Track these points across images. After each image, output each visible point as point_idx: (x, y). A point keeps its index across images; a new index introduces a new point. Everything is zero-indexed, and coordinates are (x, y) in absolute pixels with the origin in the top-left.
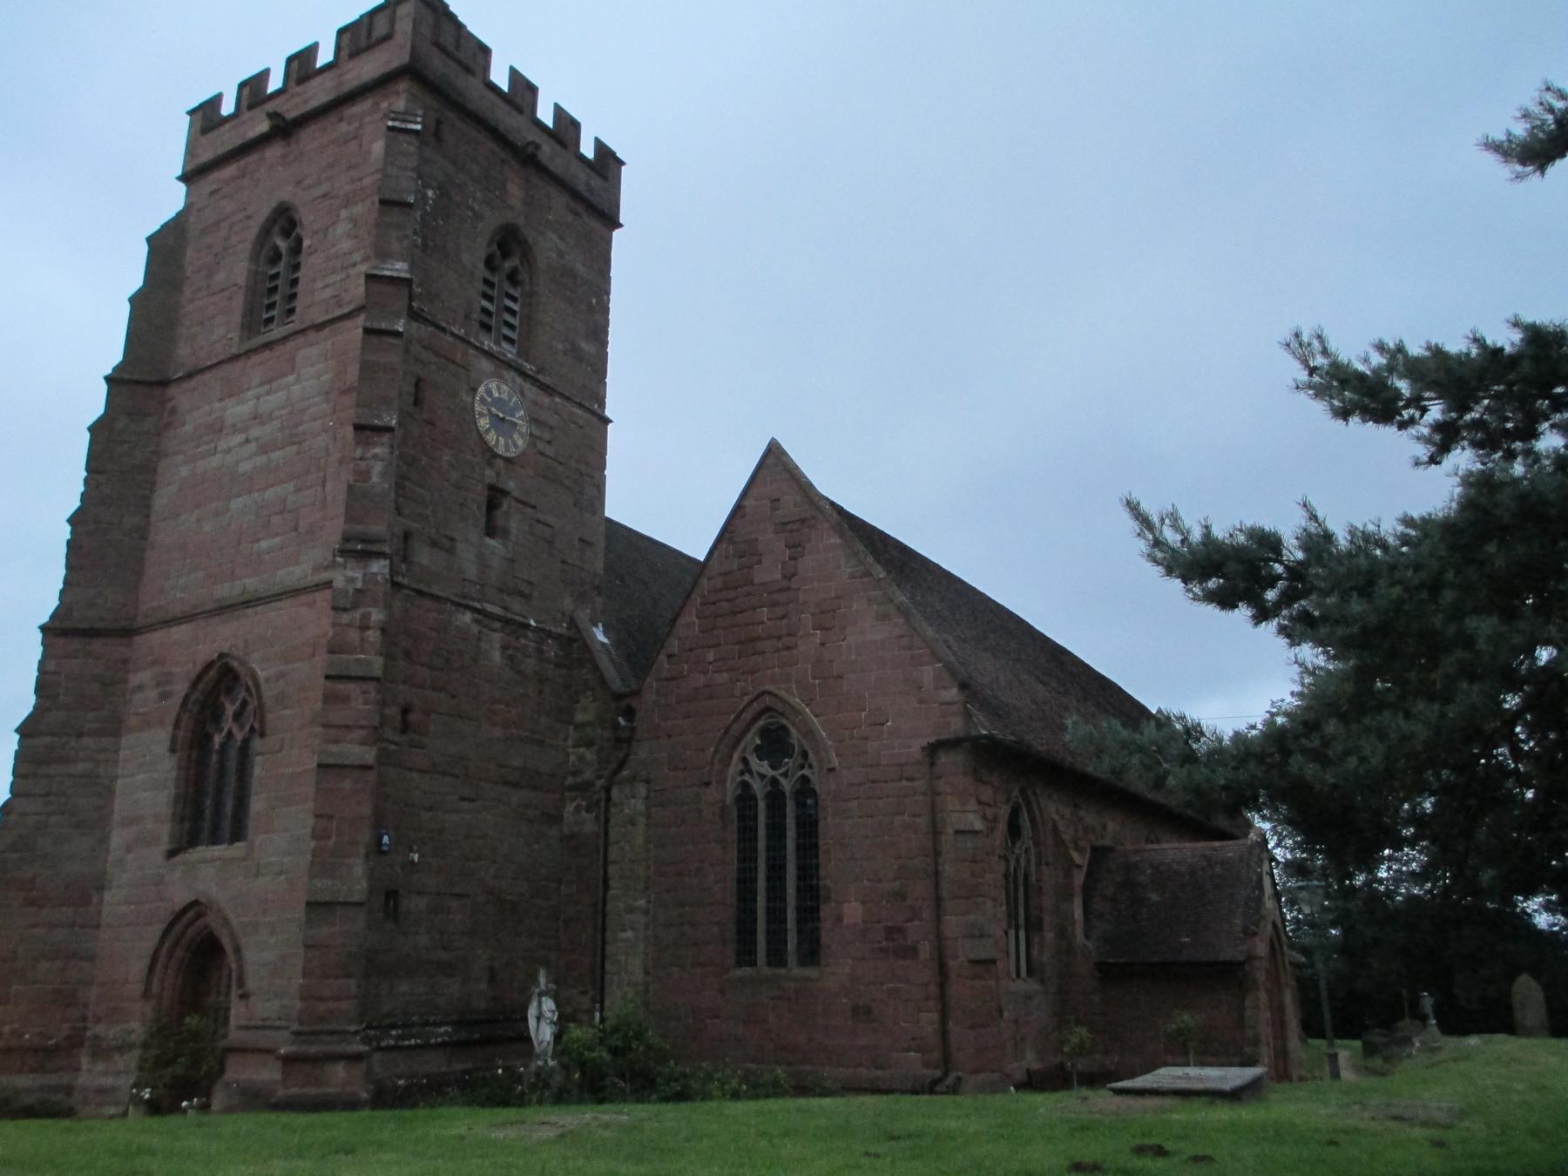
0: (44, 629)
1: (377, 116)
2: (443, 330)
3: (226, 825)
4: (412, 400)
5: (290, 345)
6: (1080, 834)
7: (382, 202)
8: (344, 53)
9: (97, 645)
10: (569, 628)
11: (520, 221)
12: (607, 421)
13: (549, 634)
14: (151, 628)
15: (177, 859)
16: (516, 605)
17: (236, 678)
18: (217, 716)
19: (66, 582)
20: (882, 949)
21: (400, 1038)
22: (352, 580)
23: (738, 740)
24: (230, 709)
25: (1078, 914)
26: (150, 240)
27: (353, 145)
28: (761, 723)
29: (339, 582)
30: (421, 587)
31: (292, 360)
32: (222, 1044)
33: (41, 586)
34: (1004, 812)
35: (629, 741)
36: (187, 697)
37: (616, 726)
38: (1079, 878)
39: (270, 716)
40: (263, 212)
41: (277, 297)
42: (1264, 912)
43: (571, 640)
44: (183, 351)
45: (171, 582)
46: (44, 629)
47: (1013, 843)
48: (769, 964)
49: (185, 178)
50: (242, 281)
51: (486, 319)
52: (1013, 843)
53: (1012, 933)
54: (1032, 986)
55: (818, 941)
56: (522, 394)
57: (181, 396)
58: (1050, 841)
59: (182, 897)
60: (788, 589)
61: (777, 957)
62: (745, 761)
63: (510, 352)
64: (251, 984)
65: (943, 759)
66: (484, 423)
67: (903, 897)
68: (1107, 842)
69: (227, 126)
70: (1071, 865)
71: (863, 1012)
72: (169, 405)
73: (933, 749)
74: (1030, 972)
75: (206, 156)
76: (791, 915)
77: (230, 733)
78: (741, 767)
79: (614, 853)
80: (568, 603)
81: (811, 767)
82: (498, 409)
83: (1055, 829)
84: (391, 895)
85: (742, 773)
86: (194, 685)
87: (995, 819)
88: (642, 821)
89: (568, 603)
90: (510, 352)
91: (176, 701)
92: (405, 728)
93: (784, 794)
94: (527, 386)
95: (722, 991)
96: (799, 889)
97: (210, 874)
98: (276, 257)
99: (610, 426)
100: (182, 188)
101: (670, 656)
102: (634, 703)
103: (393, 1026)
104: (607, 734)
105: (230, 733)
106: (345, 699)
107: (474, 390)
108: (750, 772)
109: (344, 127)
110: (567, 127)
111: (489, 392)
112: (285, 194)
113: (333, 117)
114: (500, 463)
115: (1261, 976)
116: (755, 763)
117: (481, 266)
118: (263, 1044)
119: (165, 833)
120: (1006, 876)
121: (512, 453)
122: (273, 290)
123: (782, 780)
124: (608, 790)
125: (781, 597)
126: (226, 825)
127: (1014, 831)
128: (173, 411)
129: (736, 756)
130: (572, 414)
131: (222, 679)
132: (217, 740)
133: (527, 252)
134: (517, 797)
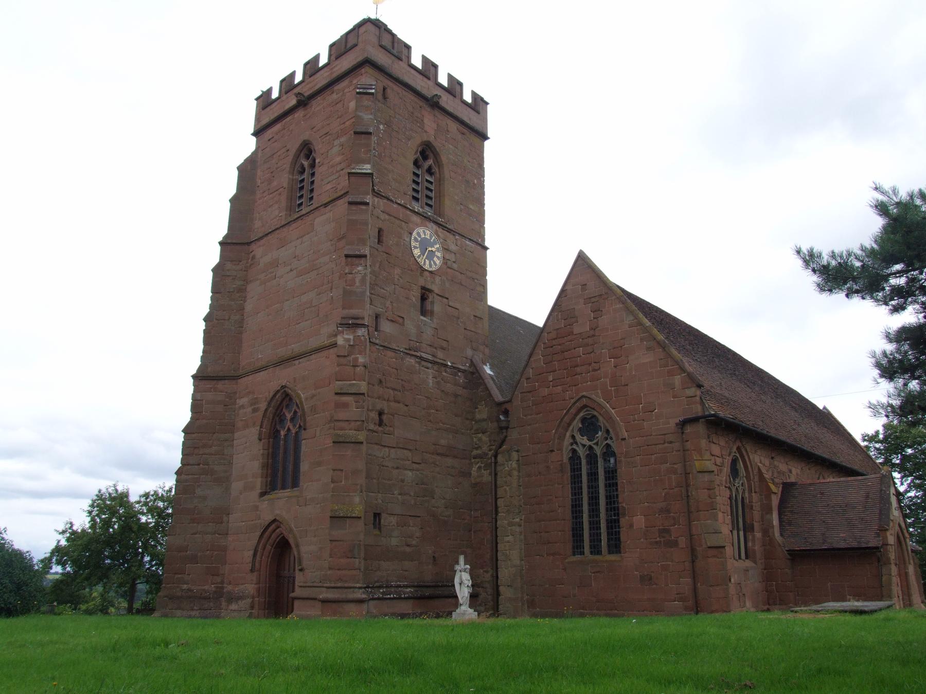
0: (194, 377)
1: (351, 88)
2: (392, 201)
3: (289, 480)
4: (376, 241)
5: (311, 216)
6: (776, 475)
7: (355, 133)
8: (333, 58)
9: (220, 385)
10: (470, 367)
11: (432, 139)
12: (486, 248)
13: (459, 370)
14: (246, 374)
15: (266, 497)
16: (440, 354)
17: (291, 399)
18: (282, 420)
19: (204, 352)
20: (656, 543)
21: (383, 593)
22: (348, 340)
23: (569, 425)
24: (289, 416)
25: (776, 522)
26: (238, 168)
27: (340, 105)
28: (582, 414)
29: (340, 340)
30: (386, 344)
31: (312, 225)
32: (292, 595)
33: (190, 353)
34: (728, 460)
35: (507, 428)
36: (266, 410)
37: (499, 420)
38: (775, 501)
39: (308, 419)
40: (294, 146)
41: (303, 192)
42: (892, 518)
43: (473, 373)
44: (257, 224)
45: (257, 351)
46: (194, 377)
47: (734, 480)
48: (591, 553)
49: (256, 134)
50: (285, 185)
51: (415, 195)
52: (734, 480)
53: (735, 532)
54: (748, 563)
55: (619, 539)
56: (438, 236)
57: (258, 250)
58: (756, 479)
59: (269, 518)
60: (594, 336)
61: (596, 549)
62: (573, 437)
63: (429, 212)
64: (305, 563)
65: (689, 429)
66: (417, 252)
67: (668, 511)
68: (793, 480)
69: (275, 104)
70: (770, 492)
71: (647, 579)
72: (251, 255)
73: (684, 423)
74: (747, 557)
75: (265, 121)
76: (603, 525)
77: (289, 429)
78: (571, 441)
79: (500, 492)
80: (469, 352)
81: (611, 438)
82: (426, 246)
83: (759, 469)
84: (377, 516)
85: (572, 444)
86: (269, 403)
87: (722, 465)
88: (515, 473)
89: (469, 352)
90: (429, 212)
91: (260, 414)
92: (381, 423)
93: (596, 455)
94: (440, 230)
95: (565, 569)
96: (607, 510)
97: (280, 505)
98: (302, 171)
99: (488, 251)
100: (254, 139)
101: (528, 379)
102: (507, 406)
103: (380, 587)
104: (495, 424)
105: (289, 429)
106: (345, 405)
107: (411, 234)
108: (576, 443)
109: (335, 96)
110: (455, 86)
111: (419, 234)
112: (306, 136)
113: (328, 92)
114: (427, 274)
115: (892, 556)
116: (578, 437)
117: (412, 165)
118: (313, 596)
119: (258, 483)
120: (730, 498)
121: (434, 268)
122: (302, 188)
123: (595, 447)
124: (496, 456)
125: (590, 341)
126: (289, 480)
127: (734, 472)
128: (253, 257)
129: (568, 434)
130: (467, 245)
131: (284, 400)
132: (282, 433)
133: (436, 156)
134: (449, 461)
